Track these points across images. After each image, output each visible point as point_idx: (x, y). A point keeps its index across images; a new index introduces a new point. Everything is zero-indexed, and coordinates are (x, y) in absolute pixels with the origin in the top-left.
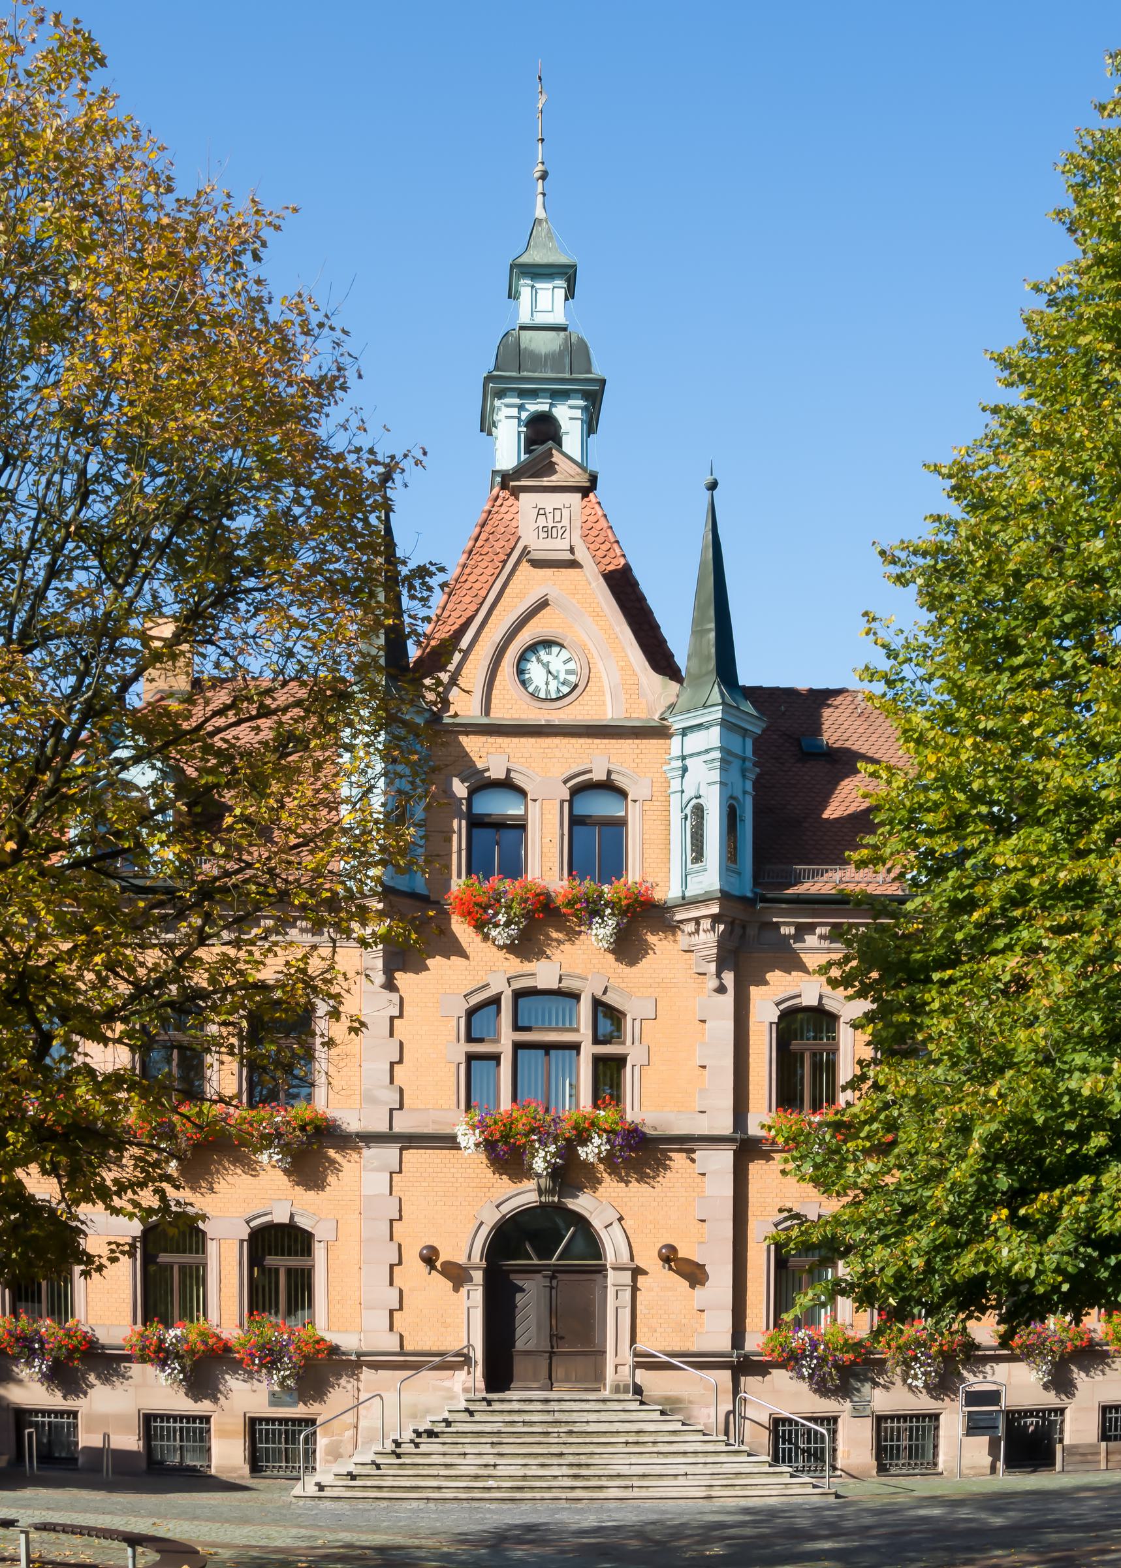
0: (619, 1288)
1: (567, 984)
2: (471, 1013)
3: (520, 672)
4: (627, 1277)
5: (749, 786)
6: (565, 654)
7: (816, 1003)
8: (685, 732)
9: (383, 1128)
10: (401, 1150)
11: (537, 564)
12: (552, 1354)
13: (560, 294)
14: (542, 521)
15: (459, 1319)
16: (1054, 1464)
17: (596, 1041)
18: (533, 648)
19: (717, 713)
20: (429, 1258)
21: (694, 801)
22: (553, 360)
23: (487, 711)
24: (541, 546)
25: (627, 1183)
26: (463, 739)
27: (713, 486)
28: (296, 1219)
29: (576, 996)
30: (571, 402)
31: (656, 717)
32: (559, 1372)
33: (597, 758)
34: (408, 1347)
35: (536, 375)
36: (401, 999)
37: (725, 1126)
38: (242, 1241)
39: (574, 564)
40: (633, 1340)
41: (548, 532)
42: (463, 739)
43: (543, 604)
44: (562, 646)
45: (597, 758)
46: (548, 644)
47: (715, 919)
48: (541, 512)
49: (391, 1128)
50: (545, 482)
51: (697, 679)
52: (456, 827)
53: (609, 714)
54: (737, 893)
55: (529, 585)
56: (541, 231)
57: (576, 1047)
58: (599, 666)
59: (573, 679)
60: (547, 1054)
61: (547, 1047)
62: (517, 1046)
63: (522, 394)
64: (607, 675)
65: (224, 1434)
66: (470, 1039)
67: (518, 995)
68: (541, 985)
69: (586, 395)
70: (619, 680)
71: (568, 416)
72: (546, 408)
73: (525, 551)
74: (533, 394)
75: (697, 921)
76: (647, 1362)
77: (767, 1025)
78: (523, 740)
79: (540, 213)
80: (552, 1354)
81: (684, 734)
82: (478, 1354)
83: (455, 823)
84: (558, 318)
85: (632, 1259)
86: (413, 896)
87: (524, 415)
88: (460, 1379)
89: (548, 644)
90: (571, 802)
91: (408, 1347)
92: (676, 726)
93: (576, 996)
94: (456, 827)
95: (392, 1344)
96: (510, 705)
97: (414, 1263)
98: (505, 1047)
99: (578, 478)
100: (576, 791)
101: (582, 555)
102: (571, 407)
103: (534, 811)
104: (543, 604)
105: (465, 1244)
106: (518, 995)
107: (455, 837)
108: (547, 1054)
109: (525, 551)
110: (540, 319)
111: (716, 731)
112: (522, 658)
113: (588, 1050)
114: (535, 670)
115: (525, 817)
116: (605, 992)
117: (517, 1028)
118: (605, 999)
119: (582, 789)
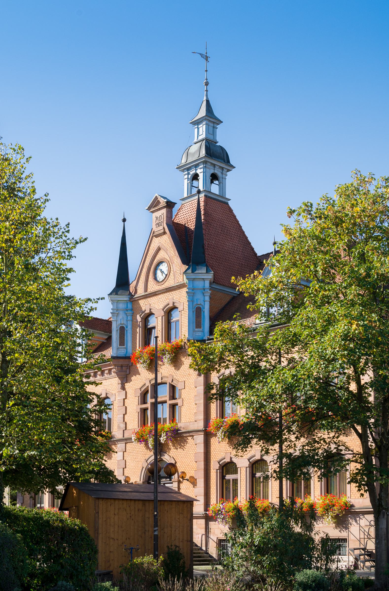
5: (207, 298)
10: (126, 443)
11: (157, 236)
25: (177, 449)
28: (233, 459)
29: (166, 383)
30: (200, 167)
36: (126, 392)
37: (200, 425)
38: (247, 467)
43: (159, 249)
49: (123, 437)
52: (138, 331)
54: (115, 356)
60: (162, 405)
72: (194, 172)
83: (138, 329)
94: (138, 331)
96: (153, 287)
107: (138, 334)
108: (162, 405)
116: (172, 381)
118: (172, 383)
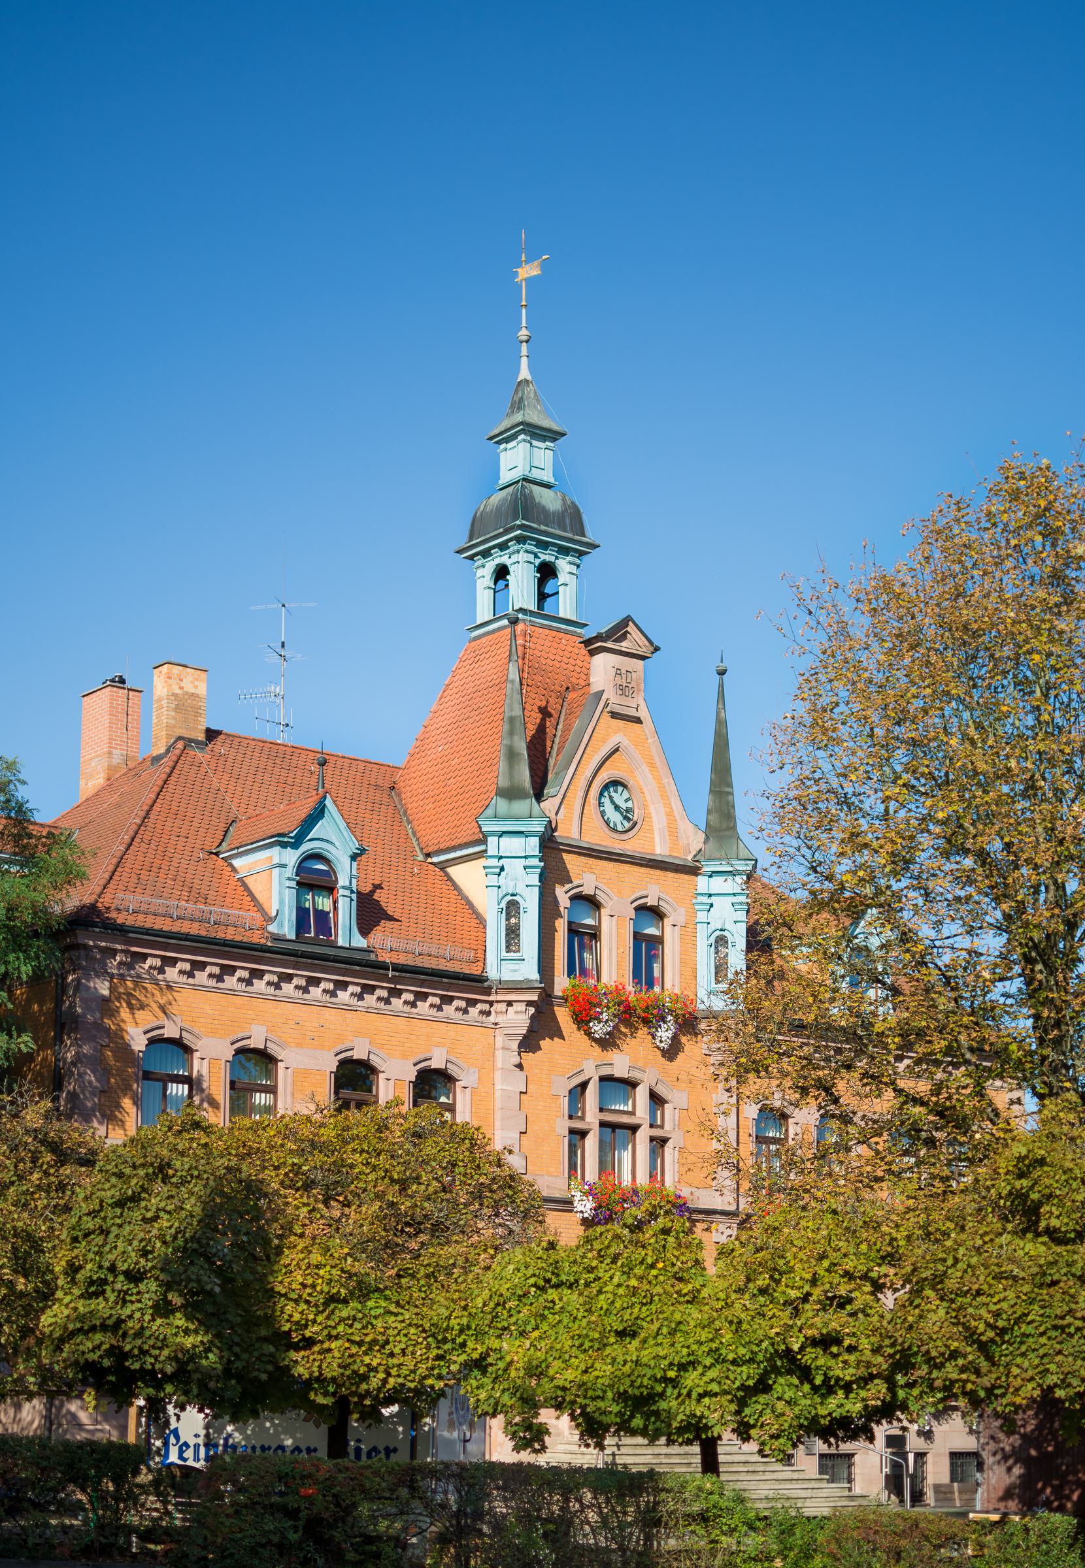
6: (626, 795)
7: (262, 1047)
11: (614, 715)
21: (718, 933)
26: (565, 856)
27: (722, 673)
29: (633, 1084)
31: (690, 858)
35: (543, 528)
39: (638, 721)
42: (565, 856)
47: (529, 1003)
53: (660, 850)
56: (530, 390)
60: (613, 1131)
68: (617, 1075)
72: (552, 559)
74: (544, 545)
75: (510, 1003)
77: (223, 1062)
78: (666, 873)
79: (524, 373)
81: (710, 876)
87: (537, 562)
89: (615, 783)
92: (706, 869)
99: (644, 649)
102: (570, 563)
108: (613, 1131)
115: (597, 928)
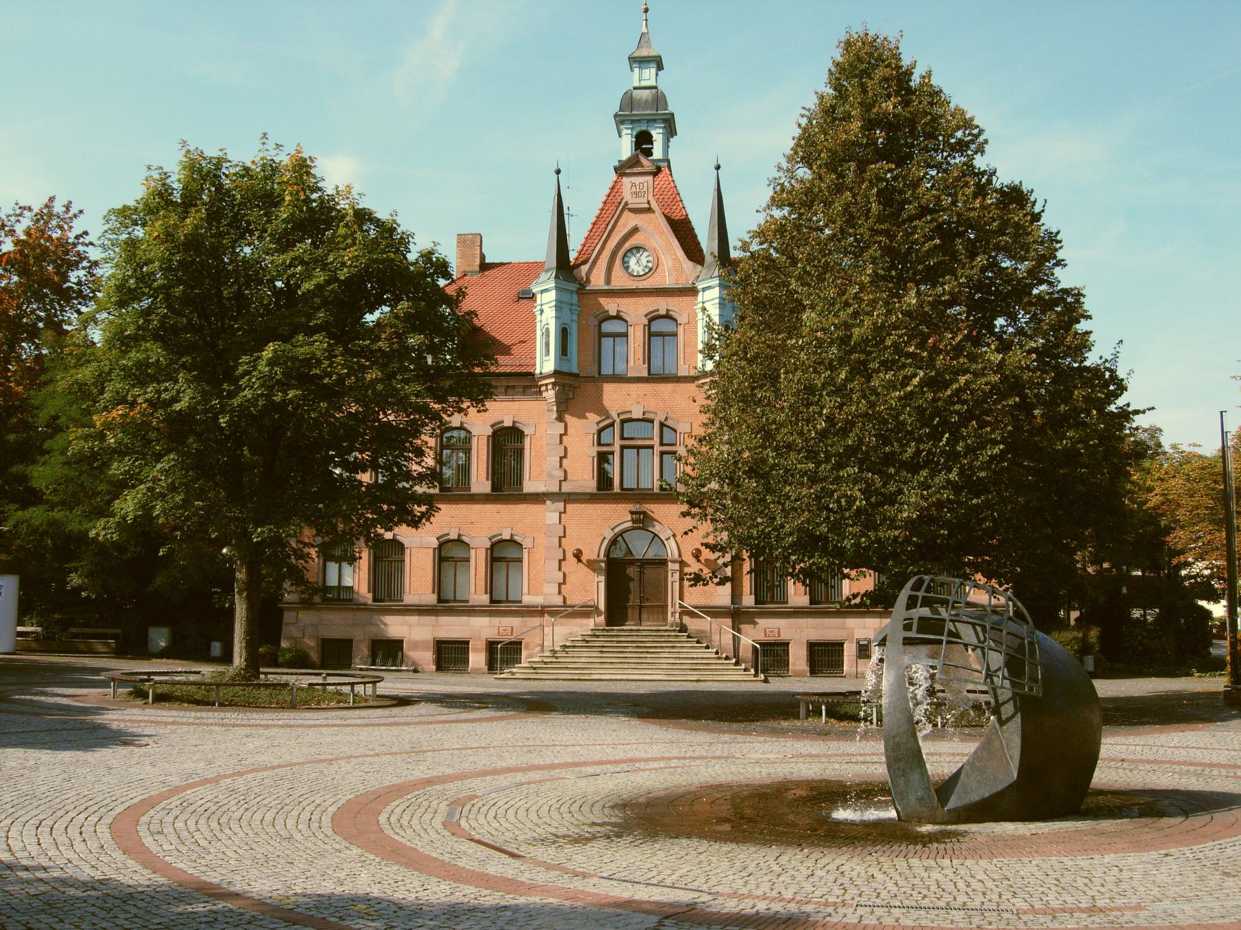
0: (674, 571)
1: (646, 416)
2: (600, 432)
3: (624, 262)
4: (677, 566)
6: (646, 254)
8: (704, 290)
9: (556, 489)
12: (641, 607)
13: (653, 70)
14: (634, 189)
15: (594, 589)
16: (840, 664)
17: (662, 444)
18: (630, 250)
19: (717, 282)
20: (578, 555)
22: (646, 105)
23: (608, 281)
24: (634, 202)
29: (652, 421)
32: (644, 616)
33: (662, 304)
34: (568, 603)
40: (681, 598)
41: (636, 194)
43: (635, 230)
44: (645, 250)
45: (662, 304)
46: (638, 248)
48: (633, 185)
50: (635, 170)
51: (710, 266)
55: (629, 221)
57: (652, 447)
58: (663, 259)
59: (650, 265)
61: (638, 448)
62: (623, 448)
63: (633, 122)
64: (666, 262)
65: (477, 650)
66: (599, 444)
67: (623, 422)
69: (665, 121)
70: (671, 264)
71: (657, 134)
73: (626, 204)
76: (685, 612)
80: (641, 607)
82: (602, 606)
84: (652, 83)
85: (680, 555)
86: (571, 375)
88: (590, 623)
89: (638, 248)
90: (649, 326)
91: (568, 603)
93: (652, 421)
95: (558, 600)
96: (620, 280)
97: (571, 559)
98: (617, 448)
100: (650, 321)
101: (654, 205)
103: (631, 330)
104: (635, 230)
105: (594, 550)
106: (623, 422)
109: (626, 204)
110: (644, 84)
111: (717, 289)
112: (625, 256)
113: (657, 449)
114: (632, 262)
117: (622, 438)
119: (653, 318)
